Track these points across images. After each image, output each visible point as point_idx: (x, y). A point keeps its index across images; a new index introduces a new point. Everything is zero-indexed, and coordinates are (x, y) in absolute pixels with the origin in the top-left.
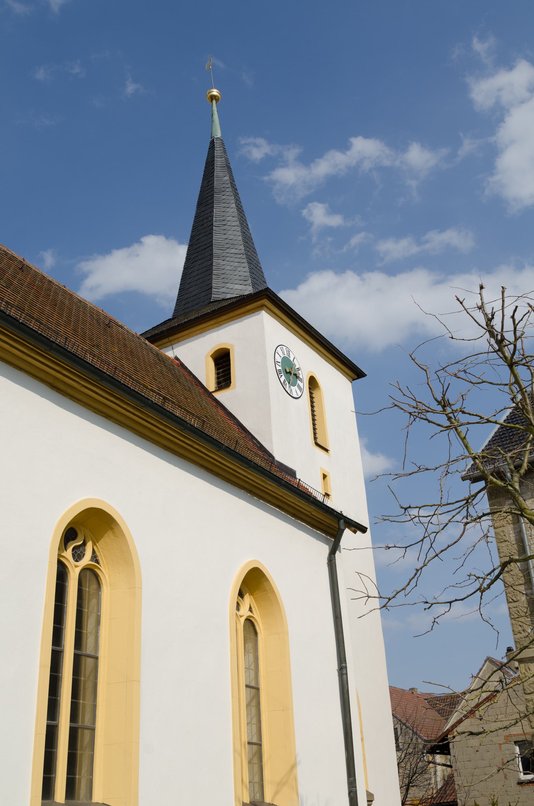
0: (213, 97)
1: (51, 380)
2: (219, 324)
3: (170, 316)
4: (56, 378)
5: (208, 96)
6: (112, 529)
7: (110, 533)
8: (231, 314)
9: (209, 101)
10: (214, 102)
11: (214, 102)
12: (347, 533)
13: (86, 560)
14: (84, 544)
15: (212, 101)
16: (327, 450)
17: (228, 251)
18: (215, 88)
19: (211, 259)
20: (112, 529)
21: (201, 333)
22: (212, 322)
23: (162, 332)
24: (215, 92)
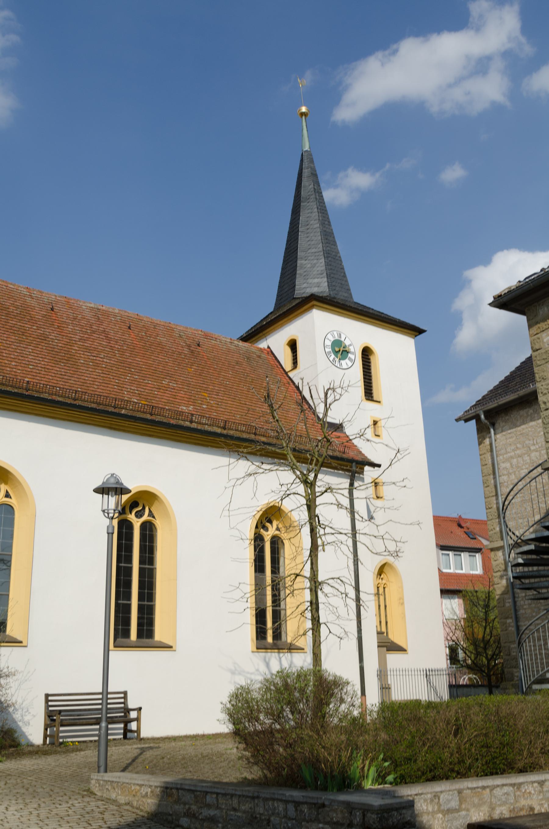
0: (302, 114)
1: (109, 425)
2: (290, 321)
3: (272, 309)
4: (111, 424)
5: (299, 114)
6: (157, 499)
7: (156, 501)
8: (299, 311)
9: (300, 117)
10: (304, 117)
11: (304, 117)
12: (367, 468)
13: (145, 517)
14: (144, 508)
15: (302, 117)
16: (379, 402)
17: (309, 251)
18: (305, 105)
19: (296, 261)
20: (157, 499)
21: (281, 327)
22: (285, 319)
23: (257, 329)
24: (304, 109)
